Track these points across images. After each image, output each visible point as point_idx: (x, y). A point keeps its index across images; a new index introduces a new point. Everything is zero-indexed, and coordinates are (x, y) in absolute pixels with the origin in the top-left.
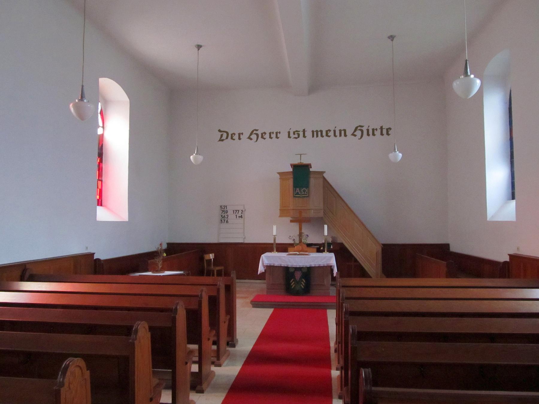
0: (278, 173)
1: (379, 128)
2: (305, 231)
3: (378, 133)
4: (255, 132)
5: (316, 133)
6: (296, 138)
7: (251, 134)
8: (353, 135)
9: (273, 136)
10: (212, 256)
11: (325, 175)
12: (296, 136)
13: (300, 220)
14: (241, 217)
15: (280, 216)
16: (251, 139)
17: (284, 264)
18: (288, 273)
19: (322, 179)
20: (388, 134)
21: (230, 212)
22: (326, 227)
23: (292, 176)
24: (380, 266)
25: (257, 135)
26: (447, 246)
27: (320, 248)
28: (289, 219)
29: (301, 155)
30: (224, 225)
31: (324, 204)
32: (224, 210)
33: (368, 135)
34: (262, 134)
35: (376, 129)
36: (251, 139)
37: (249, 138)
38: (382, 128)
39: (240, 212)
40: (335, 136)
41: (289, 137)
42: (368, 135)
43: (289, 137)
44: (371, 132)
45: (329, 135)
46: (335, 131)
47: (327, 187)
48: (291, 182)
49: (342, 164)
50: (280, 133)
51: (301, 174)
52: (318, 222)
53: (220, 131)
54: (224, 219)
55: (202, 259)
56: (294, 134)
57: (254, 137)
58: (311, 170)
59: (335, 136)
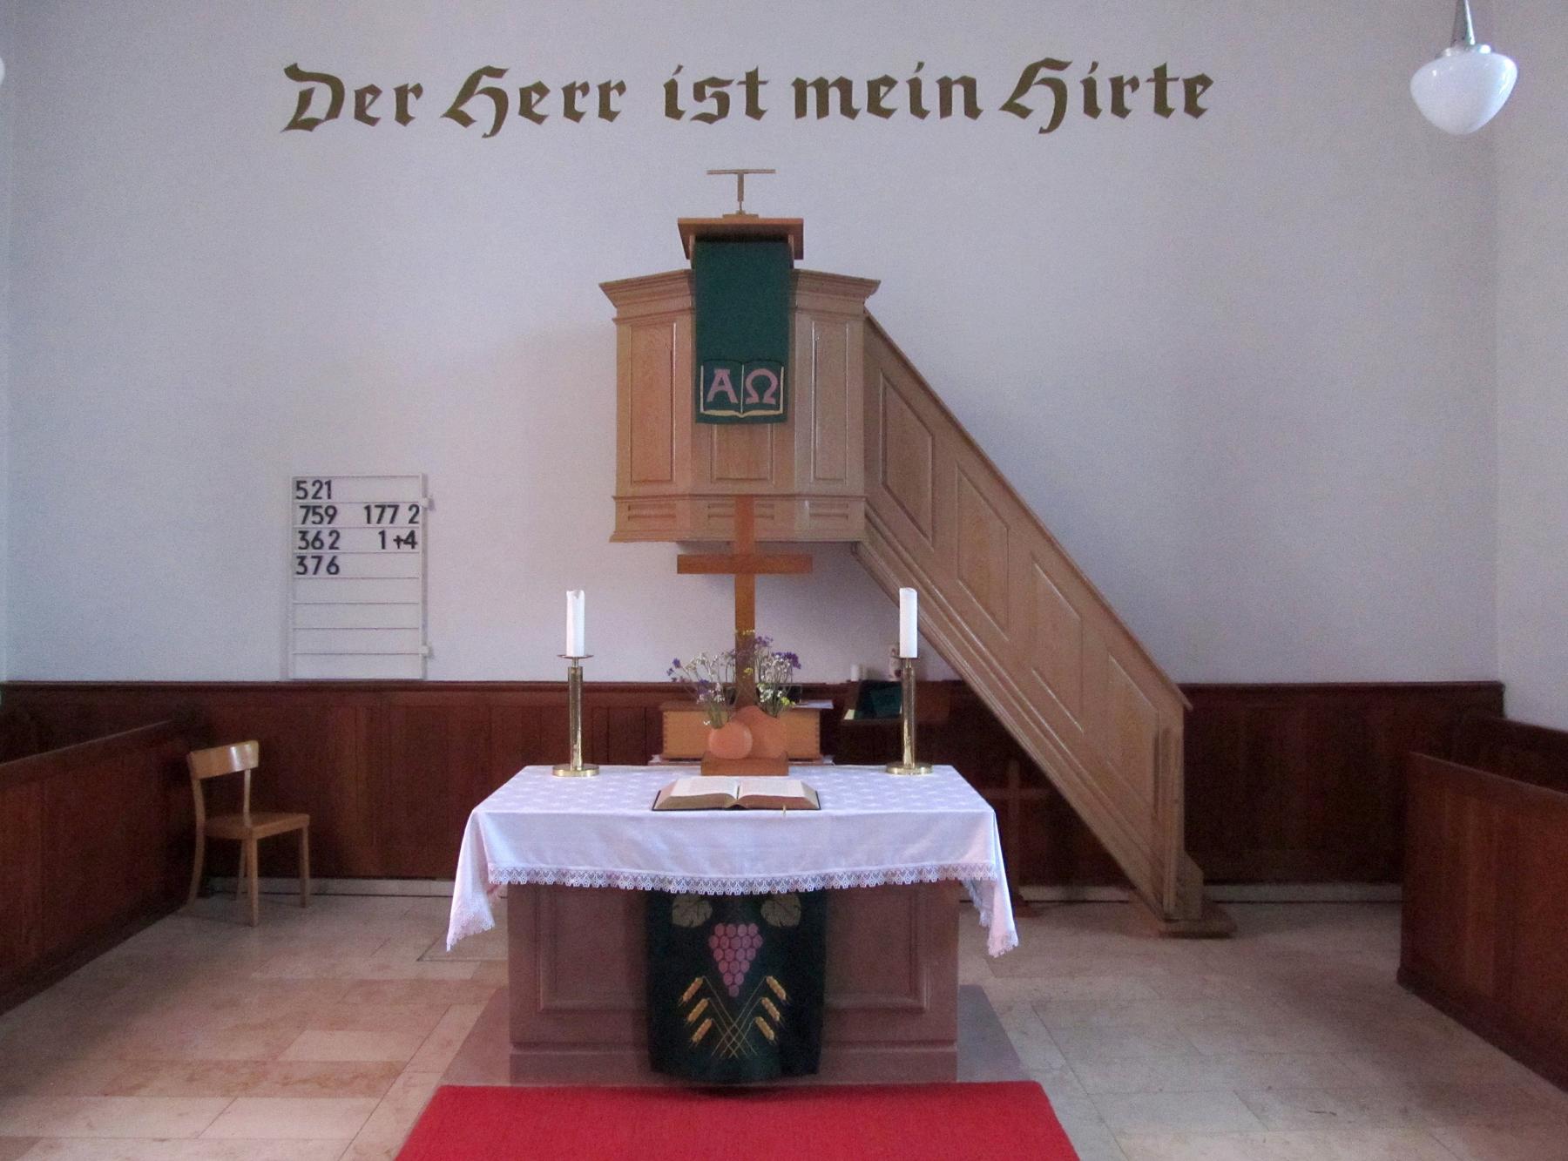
0: (608, 288)
1: (1145, 73)
2: (777, 629)
3: (1140, 100)
4: (486, 82)
5: (818, 95)
6: (706, 118)
7: (467, 91)
8: (1014, 107)
9: (588, 104)
10: (241, 757)
11: (873, 304)
12: (711, 106)
13: (734, 556)
14: (411, 540)
15: (620, 536)
16: (465, 120)
17: (633, 874)
18: (664, 934)
19: (859, 326)
20: (1193, 109)
21: (350, 517)
22: (909, 600)
23: (687, 301)
24: (1175, 813)
25: (499, 97)
26: (1485, 697)
27: (859, 728)
28: (668, 552)
29: (741, 175)
30: (318, 586)
31: (868, 468)
32: (315, 502)
33: (1091, 109)
34: (525, 94)
35: (1134, 83)
36: (465, 120)
37: (458, 115)
38: (1161, 77)
39: (404, 515)
40: (918, 110)
41: (673, 111)
42: (1091, 109)
43: (673, 111)
44: (1104, 97)
45: (885, 104)
46: (915, 85)
47: (889, 370)
48: (681, 336)
49: (965, 260)
50: (621, 88)
51: (741, 284)
52: (849, 571)
53: (294, 73)
54: (315, 551)
55: (179, 773)
56: (699, 93)
57: (481, 108)
58: (798, 265)
59: (918, 110)
